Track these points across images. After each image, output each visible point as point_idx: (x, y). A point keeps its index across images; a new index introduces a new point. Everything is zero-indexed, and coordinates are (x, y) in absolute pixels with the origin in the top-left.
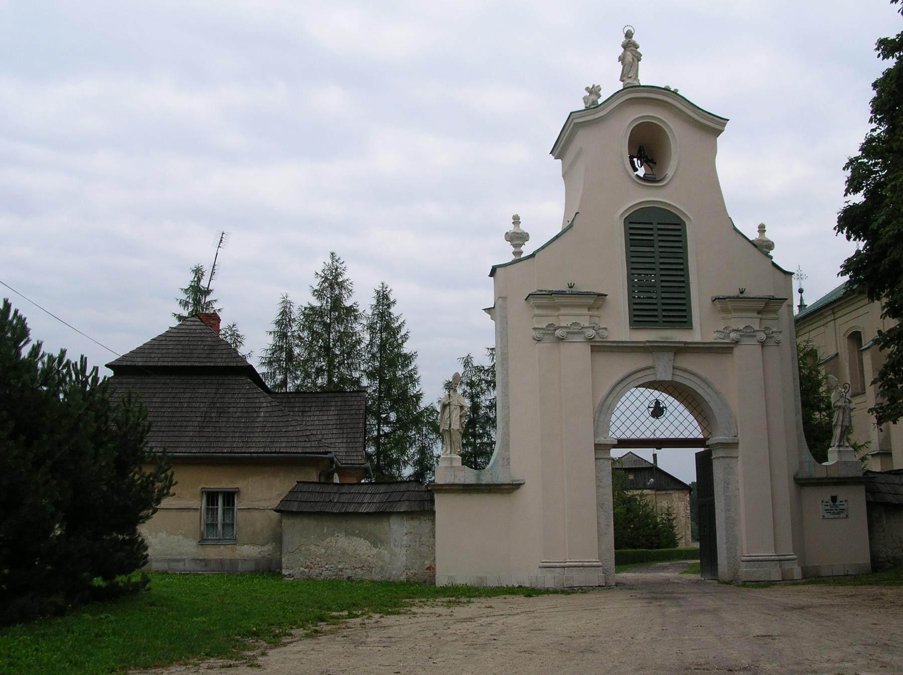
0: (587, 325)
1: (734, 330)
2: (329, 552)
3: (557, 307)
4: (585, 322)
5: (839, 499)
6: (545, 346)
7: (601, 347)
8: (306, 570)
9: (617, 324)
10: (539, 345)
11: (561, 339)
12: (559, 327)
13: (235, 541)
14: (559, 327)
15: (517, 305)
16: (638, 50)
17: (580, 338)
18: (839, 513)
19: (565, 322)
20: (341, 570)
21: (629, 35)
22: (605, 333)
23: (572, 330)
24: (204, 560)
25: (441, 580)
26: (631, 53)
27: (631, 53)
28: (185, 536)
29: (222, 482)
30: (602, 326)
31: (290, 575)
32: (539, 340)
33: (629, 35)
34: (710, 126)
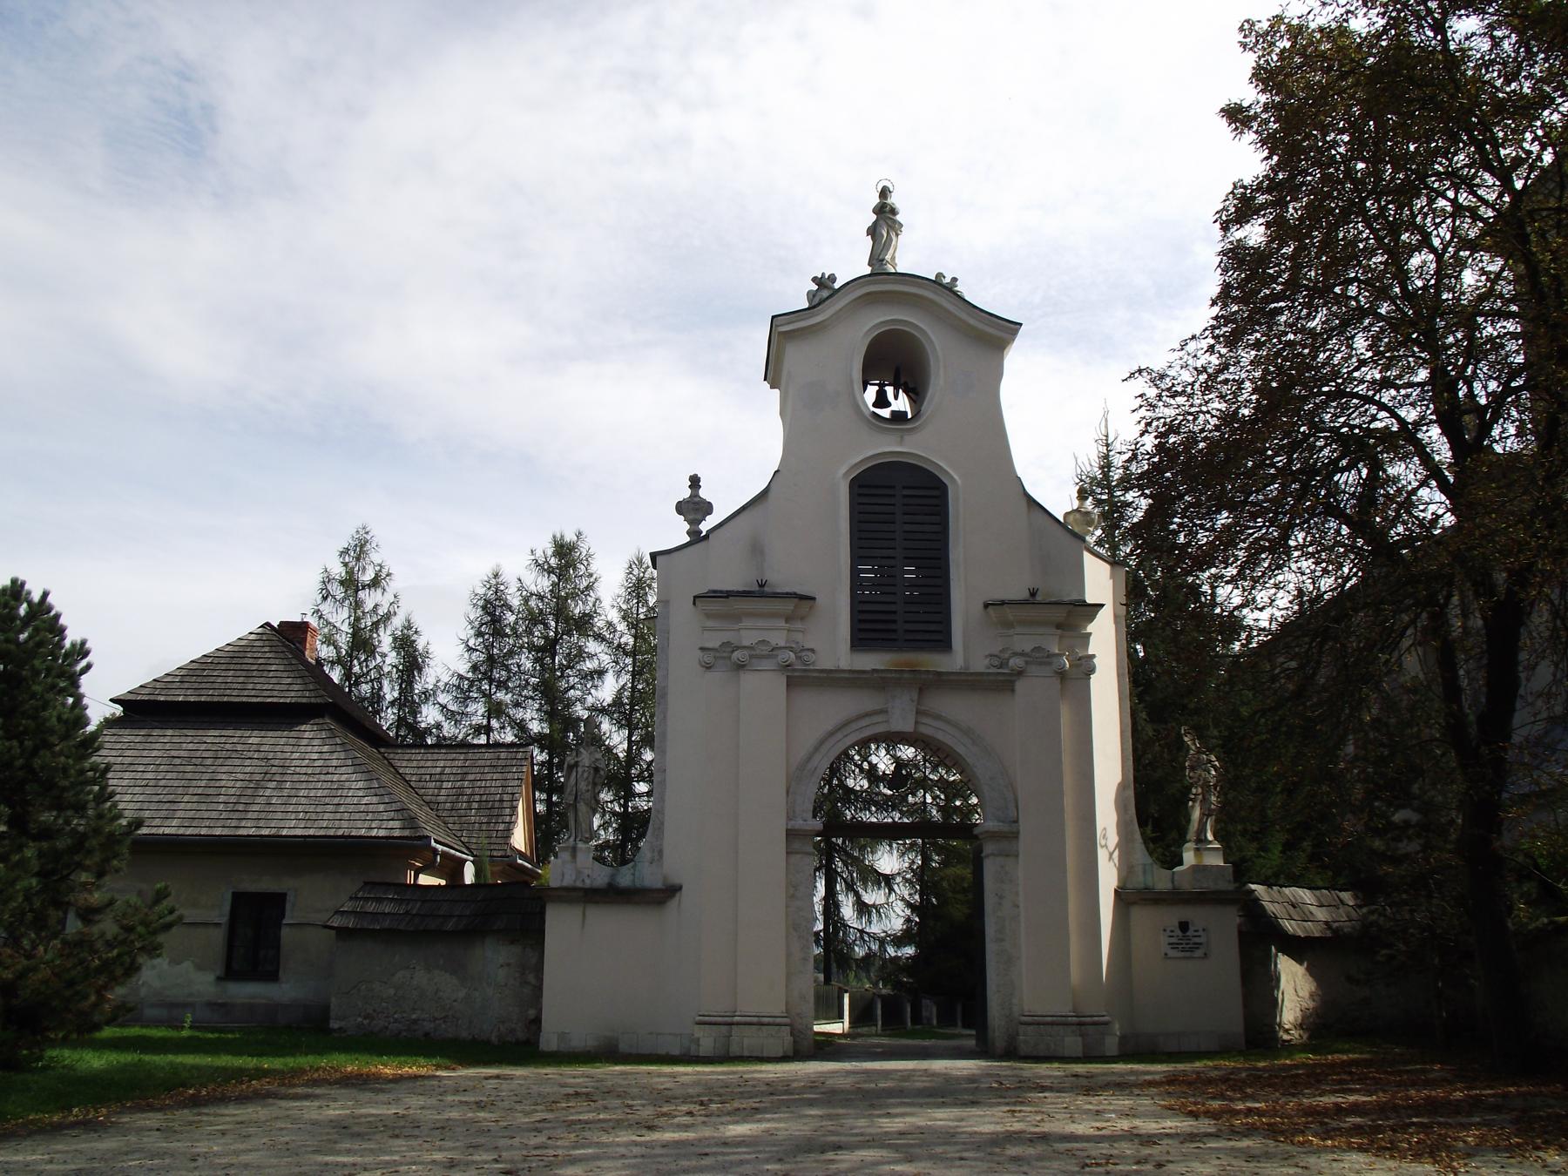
0: (782, 644)
1: (1015, 654)
3: (737, 617)
4: (778, 638)
5: (1192, 928)
7: (802, 678)
9: (831, 639)
11: (740, 667)
12: (738, 648)
13: (272, 976)
14: (738, 648)
16: (898, 218)
18: (1191, 950)
19: (749, 638)
20: (415, 1022)
21: (884, 193)
22: (812, 657)
24: (223, 1005)
26: (885, 216)
27: (885, 216)
28: (199, 967)
29: (263, 883)
30: (807, 646)
33: (884, 193)
34: (995, 334)
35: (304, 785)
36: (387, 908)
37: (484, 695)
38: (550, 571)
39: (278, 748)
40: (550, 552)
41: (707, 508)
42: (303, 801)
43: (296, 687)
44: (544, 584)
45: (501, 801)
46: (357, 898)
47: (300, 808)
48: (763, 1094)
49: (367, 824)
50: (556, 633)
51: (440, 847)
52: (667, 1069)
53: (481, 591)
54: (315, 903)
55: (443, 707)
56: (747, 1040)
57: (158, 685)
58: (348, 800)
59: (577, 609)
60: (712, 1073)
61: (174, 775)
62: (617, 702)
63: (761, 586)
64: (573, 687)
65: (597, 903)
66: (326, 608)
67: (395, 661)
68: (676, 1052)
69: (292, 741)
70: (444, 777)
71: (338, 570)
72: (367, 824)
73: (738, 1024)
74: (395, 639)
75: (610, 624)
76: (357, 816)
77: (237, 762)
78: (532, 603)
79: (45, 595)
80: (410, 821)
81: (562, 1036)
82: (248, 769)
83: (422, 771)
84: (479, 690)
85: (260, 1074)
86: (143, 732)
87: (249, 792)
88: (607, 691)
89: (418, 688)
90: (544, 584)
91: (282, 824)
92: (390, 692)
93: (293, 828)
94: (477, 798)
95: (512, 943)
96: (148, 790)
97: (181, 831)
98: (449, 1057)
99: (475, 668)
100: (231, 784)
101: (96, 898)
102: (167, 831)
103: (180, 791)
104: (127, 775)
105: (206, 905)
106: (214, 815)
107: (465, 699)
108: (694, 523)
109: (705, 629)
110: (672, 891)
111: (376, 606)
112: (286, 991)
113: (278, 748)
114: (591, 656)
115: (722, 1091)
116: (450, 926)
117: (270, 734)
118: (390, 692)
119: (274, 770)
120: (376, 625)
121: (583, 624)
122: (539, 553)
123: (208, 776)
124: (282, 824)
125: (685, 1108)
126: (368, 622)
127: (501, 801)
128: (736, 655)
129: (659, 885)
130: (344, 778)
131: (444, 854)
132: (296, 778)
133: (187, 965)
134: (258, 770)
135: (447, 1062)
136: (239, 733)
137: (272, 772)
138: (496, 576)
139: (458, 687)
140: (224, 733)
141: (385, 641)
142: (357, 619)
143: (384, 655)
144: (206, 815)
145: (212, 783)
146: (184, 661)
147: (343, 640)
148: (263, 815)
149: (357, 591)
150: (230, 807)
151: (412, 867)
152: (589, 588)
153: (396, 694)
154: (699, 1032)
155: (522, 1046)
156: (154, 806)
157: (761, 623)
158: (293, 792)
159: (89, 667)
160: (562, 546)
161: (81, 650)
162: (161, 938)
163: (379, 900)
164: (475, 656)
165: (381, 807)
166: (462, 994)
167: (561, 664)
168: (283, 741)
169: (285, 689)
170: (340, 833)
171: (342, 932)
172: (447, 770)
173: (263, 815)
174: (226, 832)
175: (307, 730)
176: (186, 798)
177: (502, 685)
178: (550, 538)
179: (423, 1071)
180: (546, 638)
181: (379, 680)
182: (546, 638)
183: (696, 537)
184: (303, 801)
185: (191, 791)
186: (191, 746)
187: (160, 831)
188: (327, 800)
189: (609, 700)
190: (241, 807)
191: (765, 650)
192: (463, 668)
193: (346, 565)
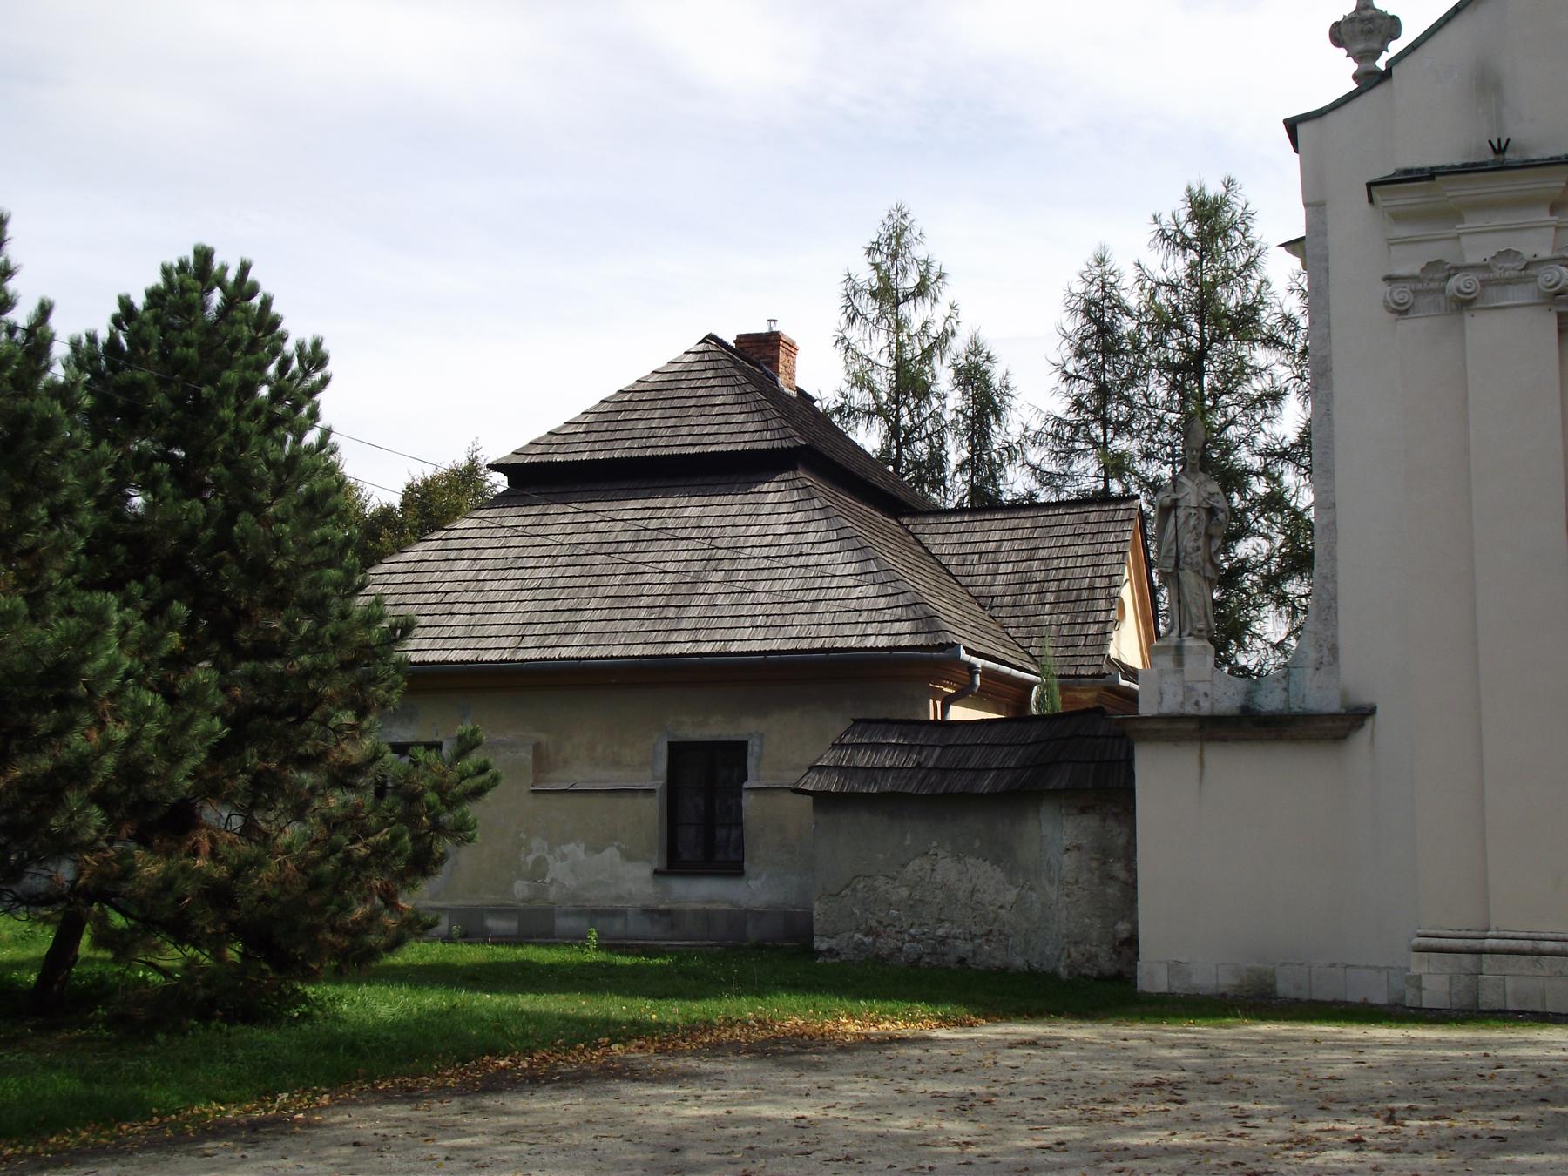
0: (1546, 253)
2: (917, 895)
3: (1453, 215)
6: (1417, 326)
8: (868, 940)
10: (1405, 325)
11: (1464, 304)
12: (1457, 269)
13: (734, 869)
14: (1457, 269)
15: (1353, 209)
17: (1517, 295)
19: (1477, 250)
20: (943, 940)
23: (1497, 274)
24: (667, 913)
25: (1152, 975)
28: (628, 856)
31: (830, 950)
32: (1402, 311)
35: (765, 575)
36: (888, 759)
37: (1096, 445)
38: (1186, 244)
39: (727, 521)
40: (1183, 216)
41: (1392, 27)
42: (763, 598)
43: (751, 427)
44: (1177, 266)
45: (1092, 588)
46: (842, 746)
47: (759, 610)
48: (1525, 1097)
49: (859, 629)
50: (1202, 340)
51: (979, 662)
52: (1355, 1032)
53: (1079, 288)
54: (788, 753)
55: (1034, 468)
56: (1510, 982)
57: (555, 440)
58: (832, 594)
59: (1231, 299)
60: (1440, 1043)
61: (577, 571)
62: (1305, 439)
63: (1499, 150)
64: (1233, 422)
65: (1223, 740)
66: (855, 334)
67: (960, 404)
68: (1380, 998)
69: (748, 509)
70: (1001, 557)
71: (866, 276)
72: (859, 629)
73: (1493, 952)
74: (958, 372)
75: (1288, 319)
76: (844, 618)
77: (668, 545)
78: (1161, 298)
79: (245, 268)
80: (927, 622)
81: (1176, 967)
82: (683, 556)
83: (967, 549)
84: (1090, 439)
85: (637, 1030)
86: (535, 510)
87: (684, 589)
88: (1289, 421)
89: (998, 438)
90: (1177, 266)
91: (730, 635)
92: (956, 452)
93: (748, 640)
94: (1053, 586)
95: (1083, 811)
96: (540, 595)
97: (585, 652)
98: (957, 1001)
99: (1078, 405)
100: (657, 578)
101: (354, 752)
102: (565, 653)
103: (585, 593)
104: (512, 574)
105: (630, 759)
106: (632, 625)
107: (1069, 454)
108: (1364, 56)
109: (1392, 242)
110: (1356, 717)
111: (925, 325)
112: (754, 892)
113: (727, 521)
114: (1258, 372)
115: (1440, 1087)
116: (984, 785)
117: (716, 500)
118: (956, 452)
119: (721, 554)
120: (927, 354)
121: (1244, 323)
122: (1166, 220)
123: (624, 569)
124: (730, 635)
125: (1350, 1127)
126: (914, 350)
127: (1092, 588)
128: (1454, 283)
129: (1334, 707)
130: (824, 559)
131: (987, 673)
132: (752, 564)
133: (611, 853)
134: (698, 555)
135: (962, 1011)
136: (670, 502)
137: (721, 556)
138: (1101, 261)
139: (1056, 436)
140: (649, 503)
141: (943, 377)
142: (900, 346)
143: (942, 397)
144: (621, 626)
145: (631, 579)
146: (592, 401)
147: (883, 380)
148: (703, 623)
149: (897, 304)
150: (656, 613)
151: (936, 694)
152: (1249, 265)
153: (965, 454)
154: (1419, 965)
155: (1106, 987)
156: (547, 617)
157: (1499, 220)
158: (749, 585)
159: (325, 381)
160: (1203, 204)
161: (315, 358)
162: (472, 810)
163: (876, 747)
164: (1077, 388)
165: (882, 602)
166: (1011, 896)
167: (1213, 389)
168: (734, 510)
169: (734, 428)
170: (818, 644)
171: (822, 800)
172: (1006, 546)
173: (703, 623)
174: (649, 650)
175: (771, 492)
176: (593, 603)
177: (1122, 427)
178: (1182, 194)
179: (900, 1028)
180: (1186, 349)
181: (940, 434)
182: (1186, 349)
183: (1368, 80)
184: (763, 598)
185: (600, 591)
186: (602, 526)
187: (556, 653)
188: (799, 595)
189: (1292, 437)
190: (671, 613)
191: (1510, 268)
192: (1060, 407)
193: (876, 267)
